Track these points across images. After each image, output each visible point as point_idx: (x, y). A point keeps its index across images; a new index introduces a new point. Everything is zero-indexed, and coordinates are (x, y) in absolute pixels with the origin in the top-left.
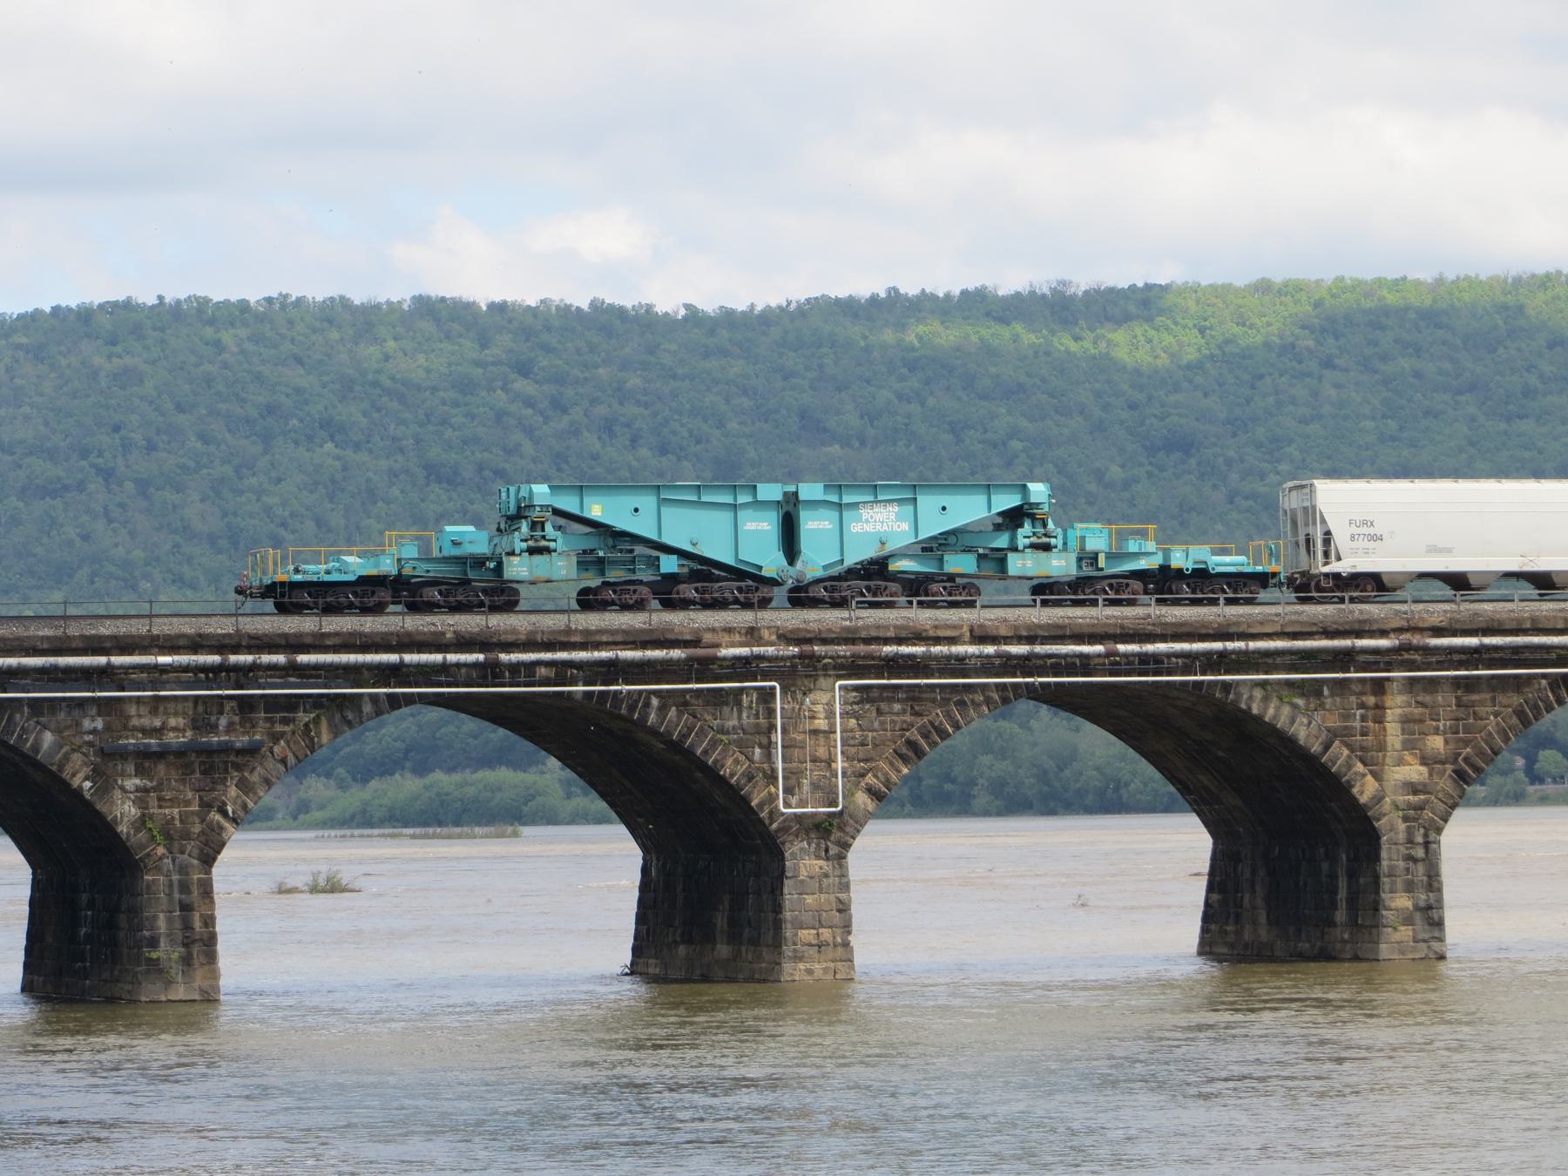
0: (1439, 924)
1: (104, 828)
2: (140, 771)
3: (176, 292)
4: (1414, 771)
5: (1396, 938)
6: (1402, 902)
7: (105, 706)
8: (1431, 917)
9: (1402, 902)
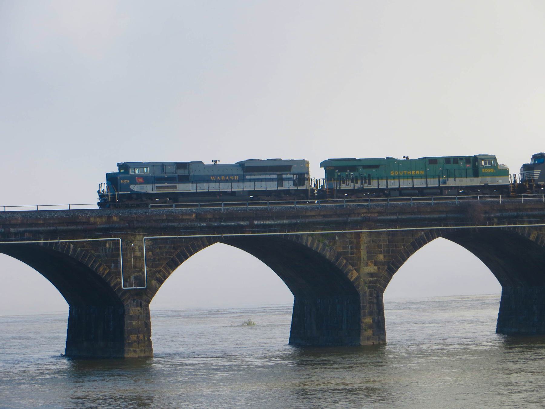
4: (372, 269)
6: (368, 320)
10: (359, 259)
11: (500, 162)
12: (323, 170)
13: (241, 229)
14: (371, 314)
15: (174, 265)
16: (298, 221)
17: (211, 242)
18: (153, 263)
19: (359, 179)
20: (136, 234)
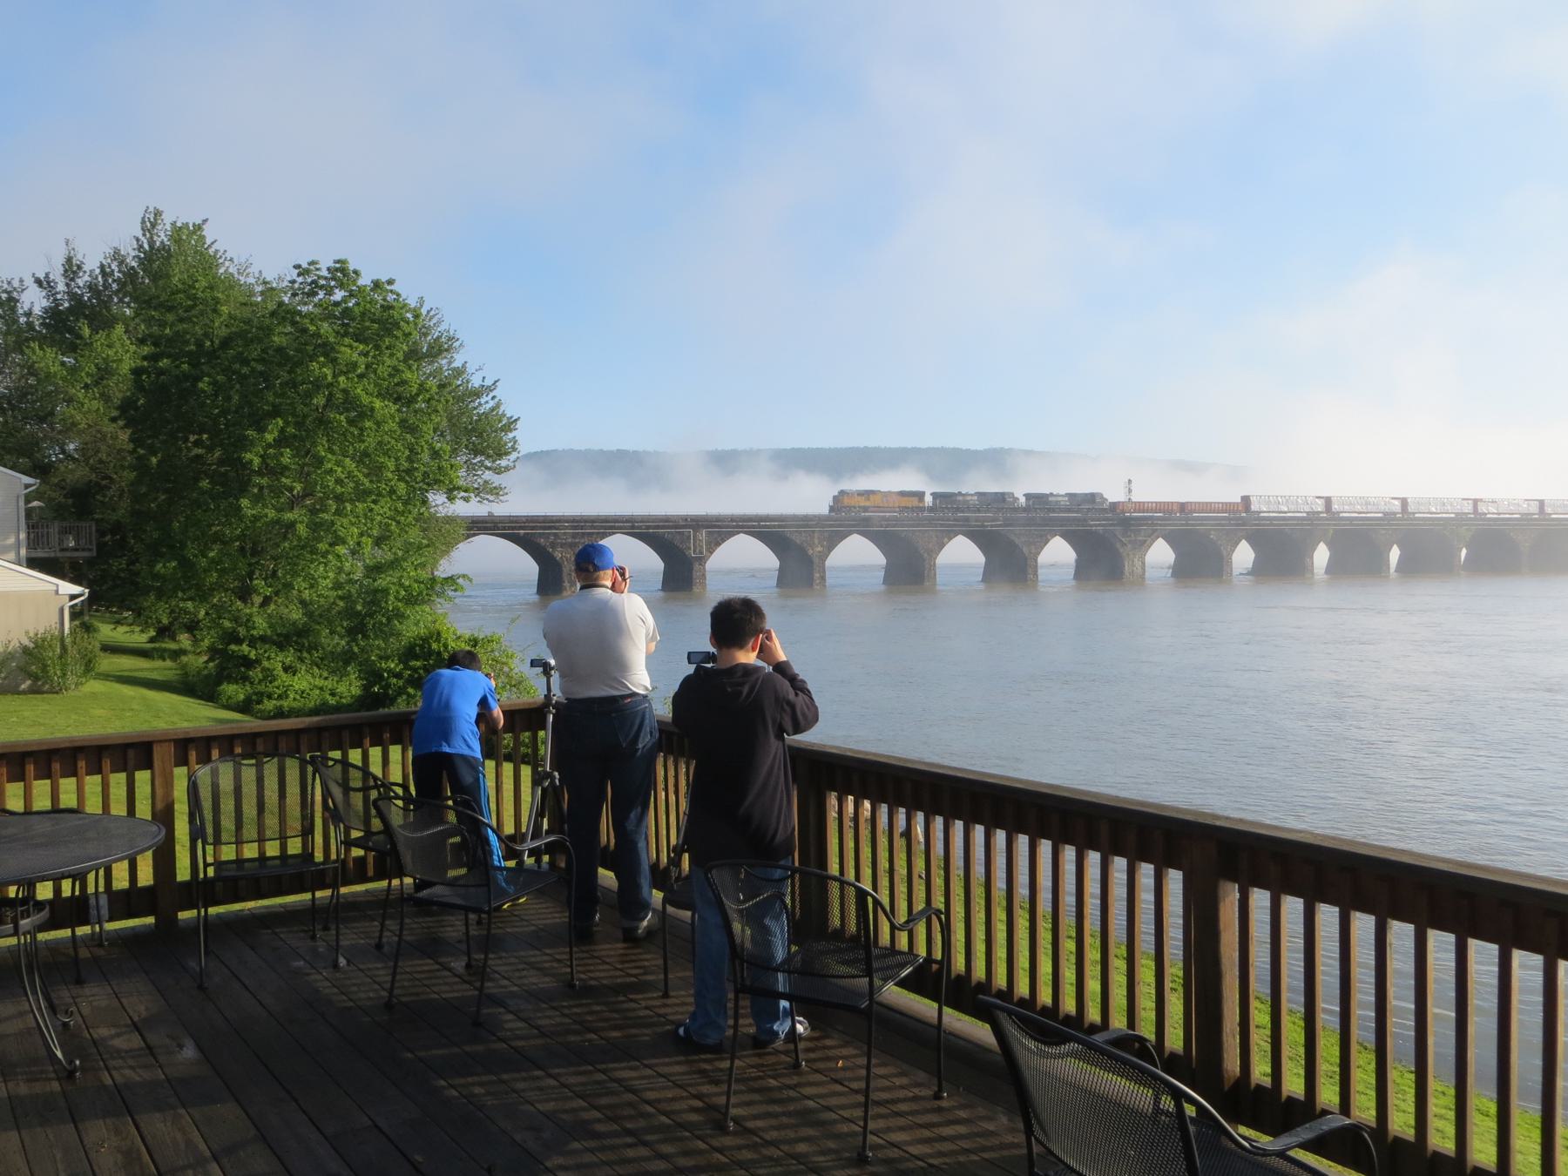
0: (825, 580)
1: (554, 558)
2: (561, 547)
3: (567, 447)
4: (819, 549)
5: (696, 589)
6: (818, 575)
7: (555, 534)
8: (823, 578)
9: (818, 575)
10: (814, 543)
11: (1105, 496)
12: (931, 497)
13: (754, 527)
14: (819, 572)
15: (718, 544)
16: (238, 366)
17: (738, 533)
18: (708, 543)
19: (157, 503)
20: (318, 944)
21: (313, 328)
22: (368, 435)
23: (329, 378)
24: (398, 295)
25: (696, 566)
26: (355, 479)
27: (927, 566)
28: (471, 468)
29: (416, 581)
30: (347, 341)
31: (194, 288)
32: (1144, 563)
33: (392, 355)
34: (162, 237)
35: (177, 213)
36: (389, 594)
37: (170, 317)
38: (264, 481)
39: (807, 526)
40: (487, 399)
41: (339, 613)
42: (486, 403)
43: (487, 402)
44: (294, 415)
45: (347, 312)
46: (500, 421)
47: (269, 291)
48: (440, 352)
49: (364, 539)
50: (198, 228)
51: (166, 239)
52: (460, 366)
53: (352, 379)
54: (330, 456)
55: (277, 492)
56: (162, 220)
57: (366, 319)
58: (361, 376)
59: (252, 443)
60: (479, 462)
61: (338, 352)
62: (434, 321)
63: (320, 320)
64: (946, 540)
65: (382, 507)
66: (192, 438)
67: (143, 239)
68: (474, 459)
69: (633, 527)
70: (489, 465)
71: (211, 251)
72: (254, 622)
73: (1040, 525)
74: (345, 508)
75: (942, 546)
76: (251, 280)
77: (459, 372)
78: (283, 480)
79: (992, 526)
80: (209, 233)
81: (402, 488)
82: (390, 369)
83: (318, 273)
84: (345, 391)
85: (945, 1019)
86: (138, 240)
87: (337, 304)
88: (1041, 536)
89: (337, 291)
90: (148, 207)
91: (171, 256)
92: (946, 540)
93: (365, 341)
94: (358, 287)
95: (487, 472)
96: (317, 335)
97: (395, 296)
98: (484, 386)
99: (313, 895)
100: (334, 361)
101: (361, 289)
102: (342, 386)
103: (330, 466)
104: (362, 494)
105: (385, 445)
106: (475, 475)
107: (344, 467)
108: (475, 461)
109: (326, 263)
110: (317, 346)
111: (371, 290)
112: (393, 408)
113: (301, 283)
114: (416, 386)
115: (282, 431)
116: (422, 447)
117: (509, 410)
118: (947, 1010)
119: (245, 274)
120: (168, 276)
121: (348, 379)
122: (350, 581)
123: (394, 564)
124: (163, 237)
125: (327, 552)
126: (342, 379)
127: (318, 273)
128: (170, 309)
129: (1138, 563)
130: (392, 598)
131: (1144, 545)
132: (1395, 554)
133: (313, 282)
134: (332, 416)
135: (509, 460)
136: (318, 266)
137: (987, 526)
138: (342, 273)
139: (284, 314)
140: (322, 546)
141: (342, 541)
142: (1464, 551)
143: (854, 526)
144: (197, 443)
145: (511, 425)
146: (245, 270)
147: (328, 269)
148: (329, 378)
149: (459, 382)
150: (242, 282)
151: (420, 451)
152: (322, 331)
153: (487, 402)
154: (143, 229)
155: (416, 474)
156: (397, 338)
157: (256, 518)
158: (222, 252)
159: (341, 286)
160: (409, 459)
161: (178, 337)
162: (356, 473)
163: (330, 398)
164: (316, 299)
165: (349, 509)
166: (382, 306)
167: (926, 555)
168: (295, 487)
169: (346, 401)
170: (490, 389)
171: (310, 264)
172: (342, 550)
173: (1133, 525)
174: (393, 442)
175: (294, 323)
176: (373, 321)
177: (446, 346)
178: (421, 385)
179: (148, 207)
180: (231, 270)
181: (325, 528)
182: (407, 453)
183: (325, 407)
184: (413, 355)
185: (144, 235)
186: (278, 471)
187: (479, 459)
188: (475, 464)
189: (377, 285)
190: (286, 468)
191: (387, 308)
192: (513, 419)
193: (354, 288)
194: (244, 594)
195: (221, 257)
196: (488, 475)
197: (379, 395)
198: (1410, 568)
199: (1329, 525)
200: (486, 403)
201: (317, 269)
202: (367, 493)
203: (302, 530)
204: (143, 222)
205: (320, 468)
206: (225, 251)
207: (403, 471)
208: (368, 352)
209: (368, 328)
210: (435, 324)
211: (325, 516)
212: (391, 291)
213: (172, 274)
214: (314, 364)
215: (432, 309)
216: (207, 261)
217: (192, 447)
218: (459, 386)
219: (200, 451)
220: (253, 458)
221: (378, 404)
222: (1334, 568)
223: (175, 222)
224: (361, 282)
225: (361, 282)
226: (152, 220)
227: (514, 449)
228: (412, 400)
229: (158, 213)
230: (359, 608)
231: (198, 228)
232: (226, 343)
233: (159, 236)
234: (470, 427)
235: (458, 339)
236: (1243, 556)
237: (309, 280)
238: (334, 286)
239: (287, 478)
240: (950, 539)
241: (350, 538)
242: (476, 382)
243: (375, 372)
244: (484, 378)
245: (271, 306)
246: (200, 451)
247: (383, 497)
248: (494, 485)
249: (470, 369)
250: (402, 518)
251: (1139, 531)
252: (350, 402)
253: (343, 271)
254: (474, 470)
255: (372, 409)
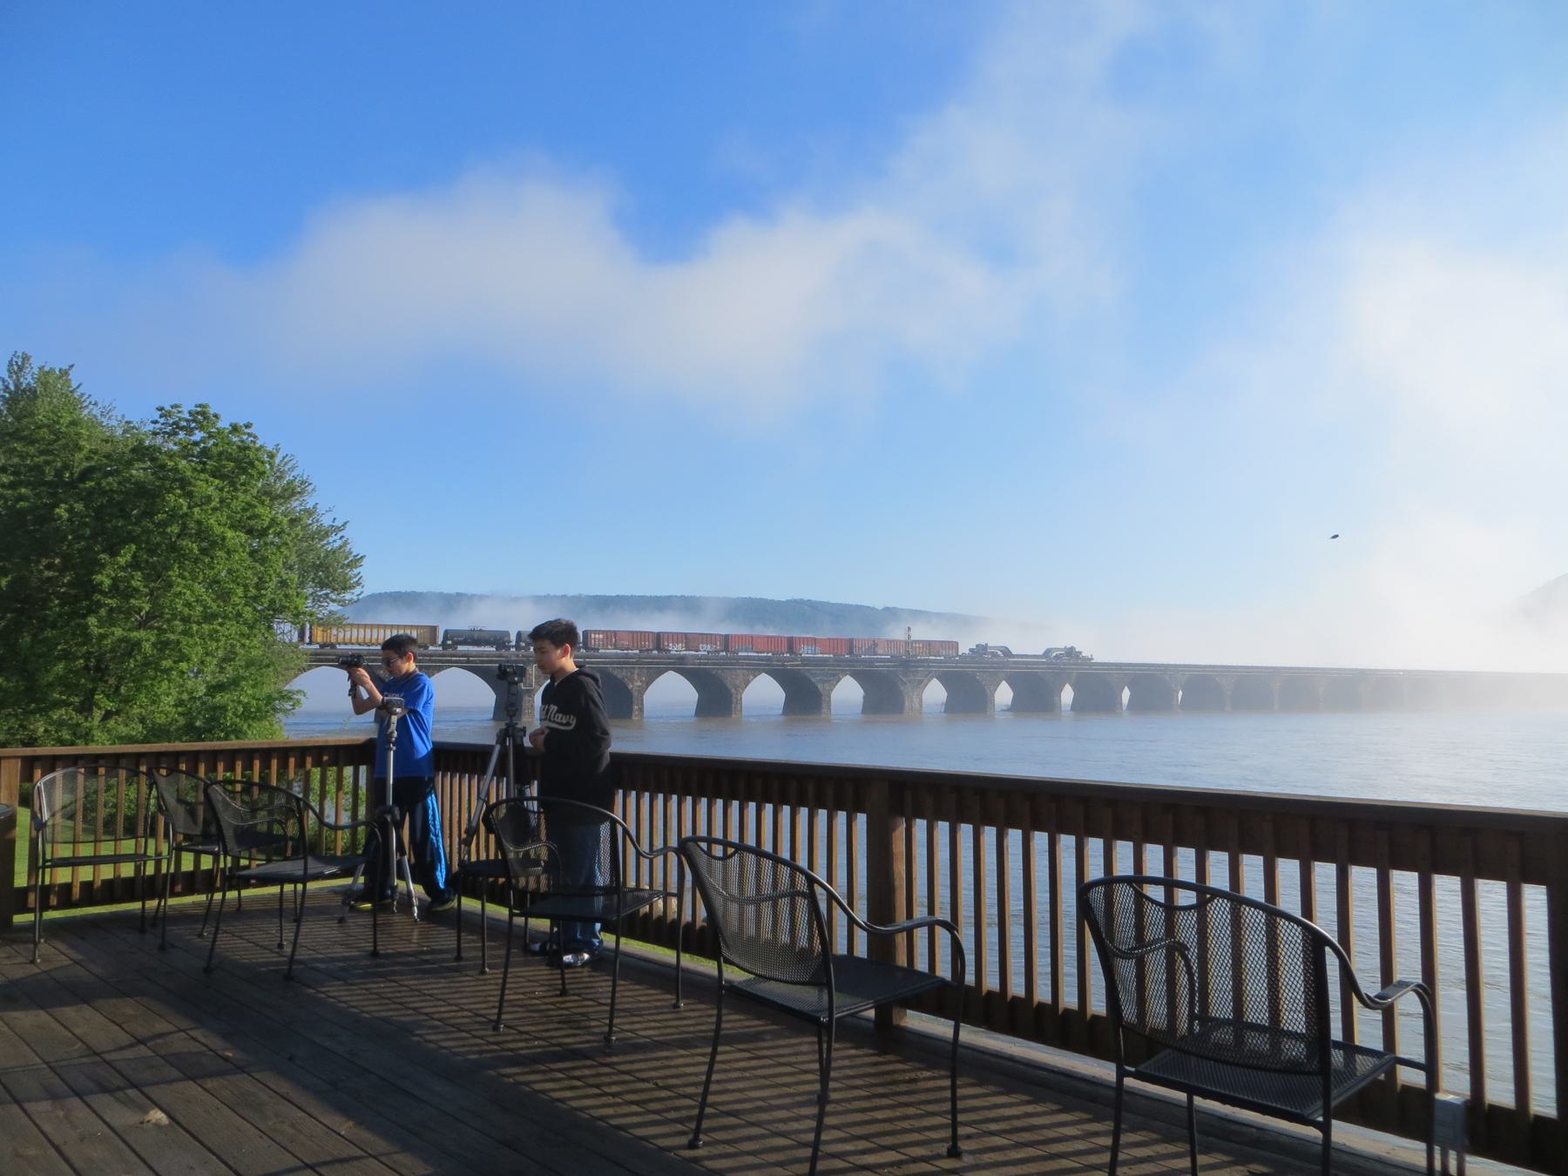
0: (643, 712)
4: (639, 684)
10: (633, 679)
21: (171, 464)
22: (218, 563)
23: (185, 508)
24: (255, 437)
25: (526, 698)
26: (204, 603)
27: (734, 700)
28: (317, 600)
29: (254, 698)
30: (203, 476)
31: (58, 423)
32: (921, 700)
33: (245, 491)
34: (28, 379)
35: (45, 357)
36: (227, 710)
37: (32, 450)
38: (112, 602)
39: (628, 663)
40: (335, 538)
41: (179, 729)
42: (334, 542)
43: (335, 541)
44: (147, 542)
45: (205, 453)
46: (347, 558)
47: (129, 427)
48: (293, 494)
49: (209, 659)
50: (64, 373)
51: (32, 382)
52: (311, 507)
53: (206, 511)
54: (179, 580)
55: (129, 612)
56: (30, 365)
57: (223, 457)
58: (215, 509)
59: (103, 566)
60: (324, 594)
61: (194, 486)
62: (289, 466)
63: (179, 456)
64: (751, 677)
65: (228, 629)
66: (44, 562)
67: (9, 380)
68: (320, 591)
69: (468, 662)
70: (334, 597)
71: (76, 395)
72: (93, 736)
73: (833, 665)
74: (190, 628)
75: (747, 683)
76: (114, 423)
77: (310, 513)
78: (132, 601)
79: (791, 666)
80: (75, 378)
81: (248, 613)
82: (243, 504)
83: (179, 415)
84: (199, 523)
85: (622, 946)
86: (3, 381)
87: (196, 444)
88: (834, 675)
89: (197, 432)
90: (16, 352)
91: (38, 397)
92: (751, 677)
93: (222, 477)
94: (217, 429)
95: (331, 604)
96: (175, 470)
97: (252, 439)
98: (333, 526)
99: (144, 905)
100: (189, 495)
101: (219, 432)
102: (196, 516)
103: (179, 589)
104: (209, 617)
105: (234, 572)
106: (320, 606)
107: (192, 591)
108: (319, 593)
109: (187, 407)
110: (175, 480)
111: (230, 432)
112: (243, 537)
113: (163, 424)
114: (268, 520)
115: (134, 557)
116: (270, 575)
117: (356, 549)
118: (623, 940)
119: (108, 417)
120: (32, 414)
121: (202, 510)
122: (192, 699)
123: (235, 683)
124: (29, 379)
125: (171, 669)
126: (196, 510)
127: (179, 415)
128: (32, 443)
129: (916, 700)
130: (230, 714)
131: (921, 684)
132: (1126, 695)
133: (174, 423)
134: (184, 543)
135: (353, 593)
136: (180, 409)
137: (787, 666)
138: (202, 416)
139: (142, 452)
140: (166, 663)
141: (184, 658)
142: (1180, 693)
143: (670, 664)
144: (49, 567)
145: (357, 561)
146: (108, 413)
147: (190, 413)
148: (185, 508)
149: (310, 522)
150: (104, 424)
151: (268, 580)
152: (180, 466)
153: (335, 541)
154: (9, 371)
155: (263, 600)
156: (252, 476)
157: (102, 637)
158: (87, 396)
159: (201, 428)
160: (257, 587)
161: (37, 469)
162: (205, 597)
163: (184, 527)
164: (176, 439)
165: (195, 629)
166: (239, 447)
167: (733, 690)
168: (144, 608)
169: (199, 533)
170: (338, 529)
171: (172, 407)
172: (183, 666)
173: (913, 667)
174: (242, 569)
175: (153, 460)
176: (229, 459)
177: (299, 490)
178: (272, 520)
179: (16, 352)
180: (94, 412)
181: (172, 646)
182: (256, 580)
183: (179, 536)
184: (268, 495)
185: (10, 377)
186: (126, 593)
187: (325, 592)
188: (321, 596)
189: (235, 429)
190: (136, 590)
191: (244, 448)
192: (359, 557)
193: (213, 430)
194: (86, 707)
195: (85, 401)
196: (333, 607)
197: (232, 527)
198: (1137, 706)
199: (1073, 669)
200: (334, 542)
201: (179, 412)
202: (214, 616)
203: (147, 646)
204: (11, 364)
205: (169, 591)
206: (90, 395)
207: (250, 598)
208: (223, 488)
209: (224, 467)
210: (289, 469)
211: (172, 637)
212: (248, 434)
213: (36, 412)
214: (171, 495)
215: (287, 455)
216: (71, 402)
217: (43, 570)
218: (310, 524)
219: (51, 574)
220: (104, 579)
221: (230, 534)
222: (1077, 706)
223: (43, 367)
224: (220, 425)
225: (220, 425)
226: (20, 363)
227: (358, 583)
228: (263, 533)
229: (26, 358)
230: (198, 724)
231: (64, 373)
232: (86, 474)
233: (26, 379)
234: (318, 562)
235: (310, 484)
236: (1004, 694)
237: (171, 421)
238: (195, 427)
239: (136, 599)
240: (755, 676)
241: (194, 656)
242: (326, 521)
243: (228, 506)
244: (335, 519)
245: (132, 443)
246: (51, 574)
247: (230, 620)
248: (338, 615)
249: (321, 510)
250: (247, 641)
251: (917, 671)
252: (202, 533)
253: (203, 414)
254: (319, 601)
255: (224, 539)
